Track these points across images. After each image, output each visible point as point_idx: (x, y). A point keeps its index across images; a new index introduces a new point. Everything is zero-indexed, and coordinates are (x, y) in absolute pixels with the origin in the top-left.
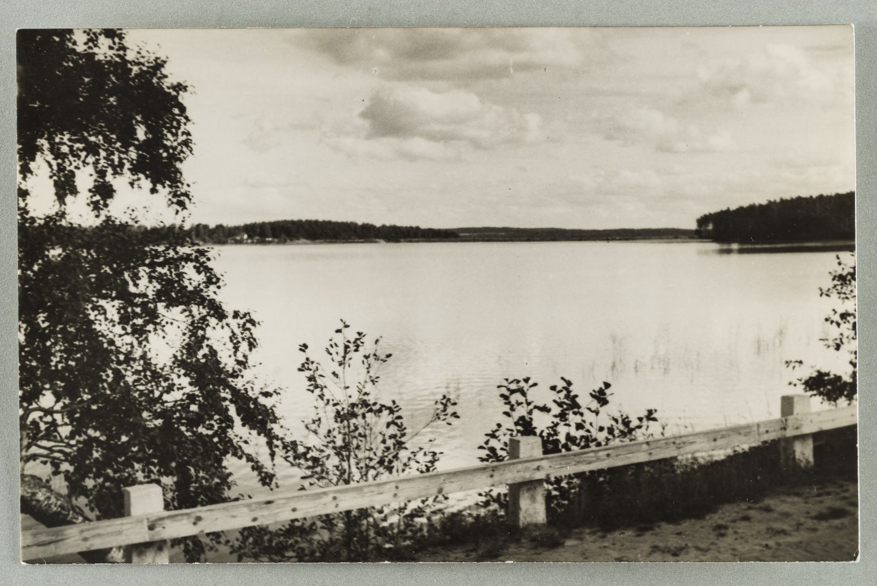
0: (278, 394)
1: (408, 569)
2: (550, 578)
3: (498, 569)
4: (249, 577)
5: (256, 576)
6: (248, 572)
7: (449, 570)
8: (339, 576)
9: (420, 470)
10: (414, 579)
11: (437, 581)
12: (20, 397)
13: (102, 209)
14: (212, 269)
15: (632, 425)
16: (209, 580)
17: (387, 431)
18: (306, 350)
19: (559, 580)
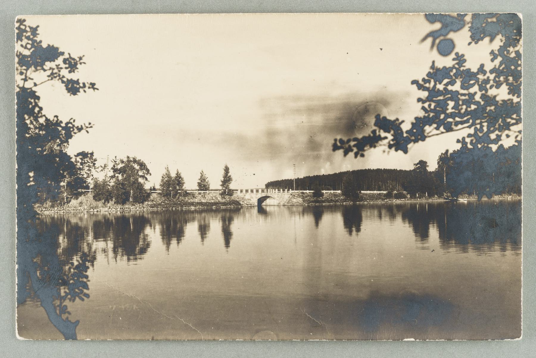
0: (434, 251)
1: (157, 344)
2: (244, 349)
3: (211, 344)
4: (60, 349)
5: (64, 349)
6: (59, 346)
7: (182, 345)
8: (114, 348)
9: (142, 259)
10: (160, 350)
11: (174, 351)
12: (309, 176)
13: (121, 179)
14: (38, 98)
15: (117, 163)
16: (35, 351)
17: (82, 223)
18: (90, 152)
19: (249, 350)
